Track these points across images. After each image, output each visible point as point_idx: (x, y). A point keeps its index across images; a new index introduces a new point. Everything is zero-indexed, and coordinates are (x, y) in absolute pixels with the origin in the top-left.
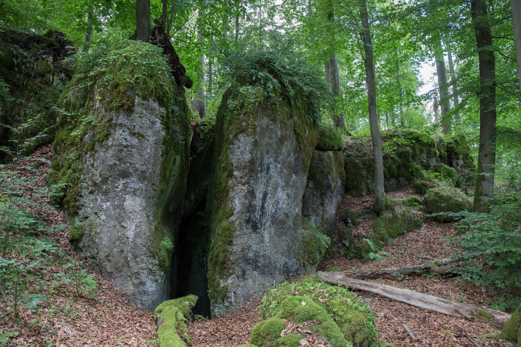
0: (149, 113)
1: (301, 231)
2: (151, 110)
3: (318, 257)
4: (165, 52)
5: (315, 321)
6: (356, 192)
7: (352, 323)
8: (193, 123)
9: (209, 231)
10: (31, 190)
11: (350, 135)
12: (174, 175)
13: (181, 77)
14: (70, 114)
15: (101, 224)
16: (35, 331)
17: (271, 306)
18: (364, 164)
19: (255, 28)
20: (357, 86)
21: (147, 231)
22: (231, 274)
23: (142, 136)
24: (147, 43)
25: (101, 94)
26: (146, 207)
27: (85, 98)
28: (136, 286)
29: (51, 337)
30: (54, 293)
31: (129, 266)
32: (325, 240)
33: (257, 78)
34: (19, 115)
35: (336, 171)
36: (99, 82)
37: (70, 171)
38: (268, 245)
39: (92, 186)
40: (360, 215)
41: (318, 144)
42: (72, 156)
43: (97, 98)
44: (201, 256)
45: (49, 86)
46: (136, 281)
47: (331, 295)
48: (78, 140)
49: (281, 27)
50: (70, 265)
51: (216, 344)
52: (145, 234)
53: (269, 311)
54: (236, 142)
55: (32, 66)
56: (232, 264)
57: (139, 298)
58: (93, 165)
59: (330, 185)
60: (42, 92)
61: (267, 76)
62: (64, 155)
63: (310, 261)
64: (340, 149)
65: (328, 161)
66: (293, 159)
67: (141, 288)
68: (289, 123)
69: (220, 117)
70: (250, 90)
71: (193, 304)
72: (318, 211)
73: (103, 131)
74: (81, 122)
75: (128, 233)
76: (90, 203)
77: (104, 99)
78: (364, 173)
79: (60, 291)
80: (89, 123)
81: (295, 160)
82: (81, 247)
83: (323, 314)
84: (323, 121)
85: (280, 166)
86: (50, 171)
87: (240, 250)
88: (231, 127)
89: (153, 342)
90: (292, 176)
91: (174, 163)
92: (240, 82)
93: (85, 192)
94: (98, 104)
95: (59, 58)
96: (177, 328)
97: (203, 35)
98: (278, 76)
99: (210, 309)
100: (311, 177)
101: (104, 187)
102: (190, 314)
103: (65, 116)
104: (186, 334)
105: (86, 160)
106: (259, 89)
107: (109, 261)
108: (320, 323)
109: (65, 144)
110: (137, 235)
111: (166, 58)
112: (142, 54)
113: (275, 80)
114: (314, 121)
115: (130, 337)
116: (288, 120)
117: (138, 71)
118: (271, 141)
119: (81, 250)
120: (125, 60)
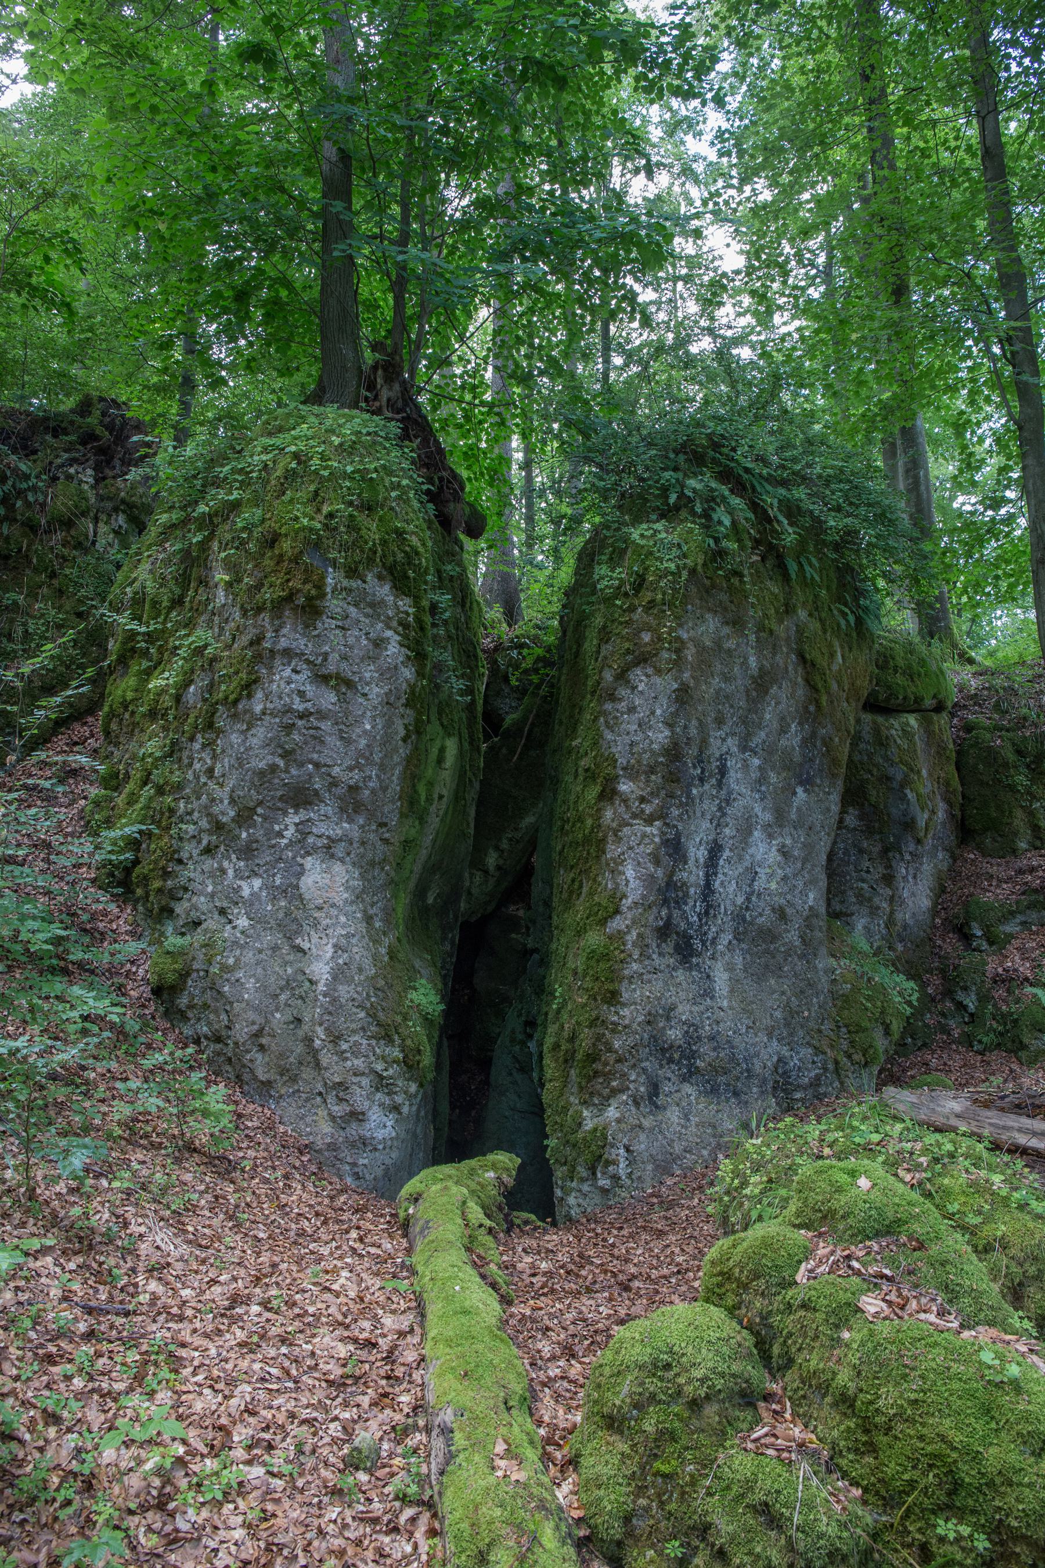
0: (367, 616)
1: (824, 961)
2: (372, 605)
3: (881, 1043)
4: (405, 436)
5: (903, 1239)
6: (994, 840)
7: (1013, 1252)
8: (487, 643)
9: (544, 963)
10: (47, 845)
11: (971, 661)
12: (441, 797)
13: (452, 505)
14: (143, 629)
15: (235, 943)
16: (81, 1239)
17: (747, 1191)
18: (1019, 752)
19: (660, 349)
20: (991, 507)
21: (367, 963)
22: (615, 1092)
23: (349, 684)
24: (355, 412)
25: (230, 566)
26: (363, 891)
27: (184, 580)
28: (342, 1122)
29: (124, 1258)
30: (121, 1137)
31: (318, 1065)
32: (901, 990)
33: (682, 495)
34: (10, 638)
35: (930, 775)
36: (224, 532)
37: (148, 791)
38: (725, 1004)
39: (210, 832)
40: (1012, 914)
41: (873, 694)
42: (153, 746)
43: (218, 577)
44: (520, 1037)
45: (86, 551)
46: (338, 1110)
47: (936, 1160)
48: (167, 701)
49: (739, 341)
50: (159, 1058)
51: (584, 1300)
52: (360, 970)
53: (742, 1204)
54: (623, 692)
55: (41, 499)
56: (619, 1061)
57: (349, 1160)
58: (210, 772)
59: (913, 820)
60: (67, 571)
61: (712, 490)
62: (132, 746)
63: (855, 1057)
64: (939, 708)
65: (903, 744)
66: (796, 741)
67: (354, 1130)
68: (783, 629)
69: (574, 620)
70: (663, 535)
71: (509, 1180)
72: (876, 900)
73: (237, 673)
74: (176, 648)
75: (313, 967)
76: (203, 881)
77: (239, 581)
78: (1021, 779)
79: (135, 1133)
80: (199, 651)
81: (804, 741)
82: (182, 1006)
83: (927, 1220)
84: (884, 620)
85: (756, 762)
86: (94, 791)
87: (641, 1018)
88: (606, 649)
89: (404, 1285)
90: (795, 793)
91: (440, 760)
92: (630, 511)
93: (189, 849)
94: (221, 597)
95: (110, 474)
96: (468, 1249)
97: (511, 377)
98: (744, 488)
99: (552, 1193)
100: (854, 795)
101: (244, 835)
102: (500, 1208)
103: (132, 635)
104: (493, 1267)
105: (191, 758)
106: (691, 531)
107: (262, 1048)
108: (921, 1246)
109: (133, 713)
110: (339, 975)
111: (411, 449)
112: (341, 445)
113: (736, 501)
114: (859, 621)
115: (335, 1271)
116: (781, 621)
117: (332, 495)
118: (729, 688)
119: (184, 1017)
120: (294, 465)
